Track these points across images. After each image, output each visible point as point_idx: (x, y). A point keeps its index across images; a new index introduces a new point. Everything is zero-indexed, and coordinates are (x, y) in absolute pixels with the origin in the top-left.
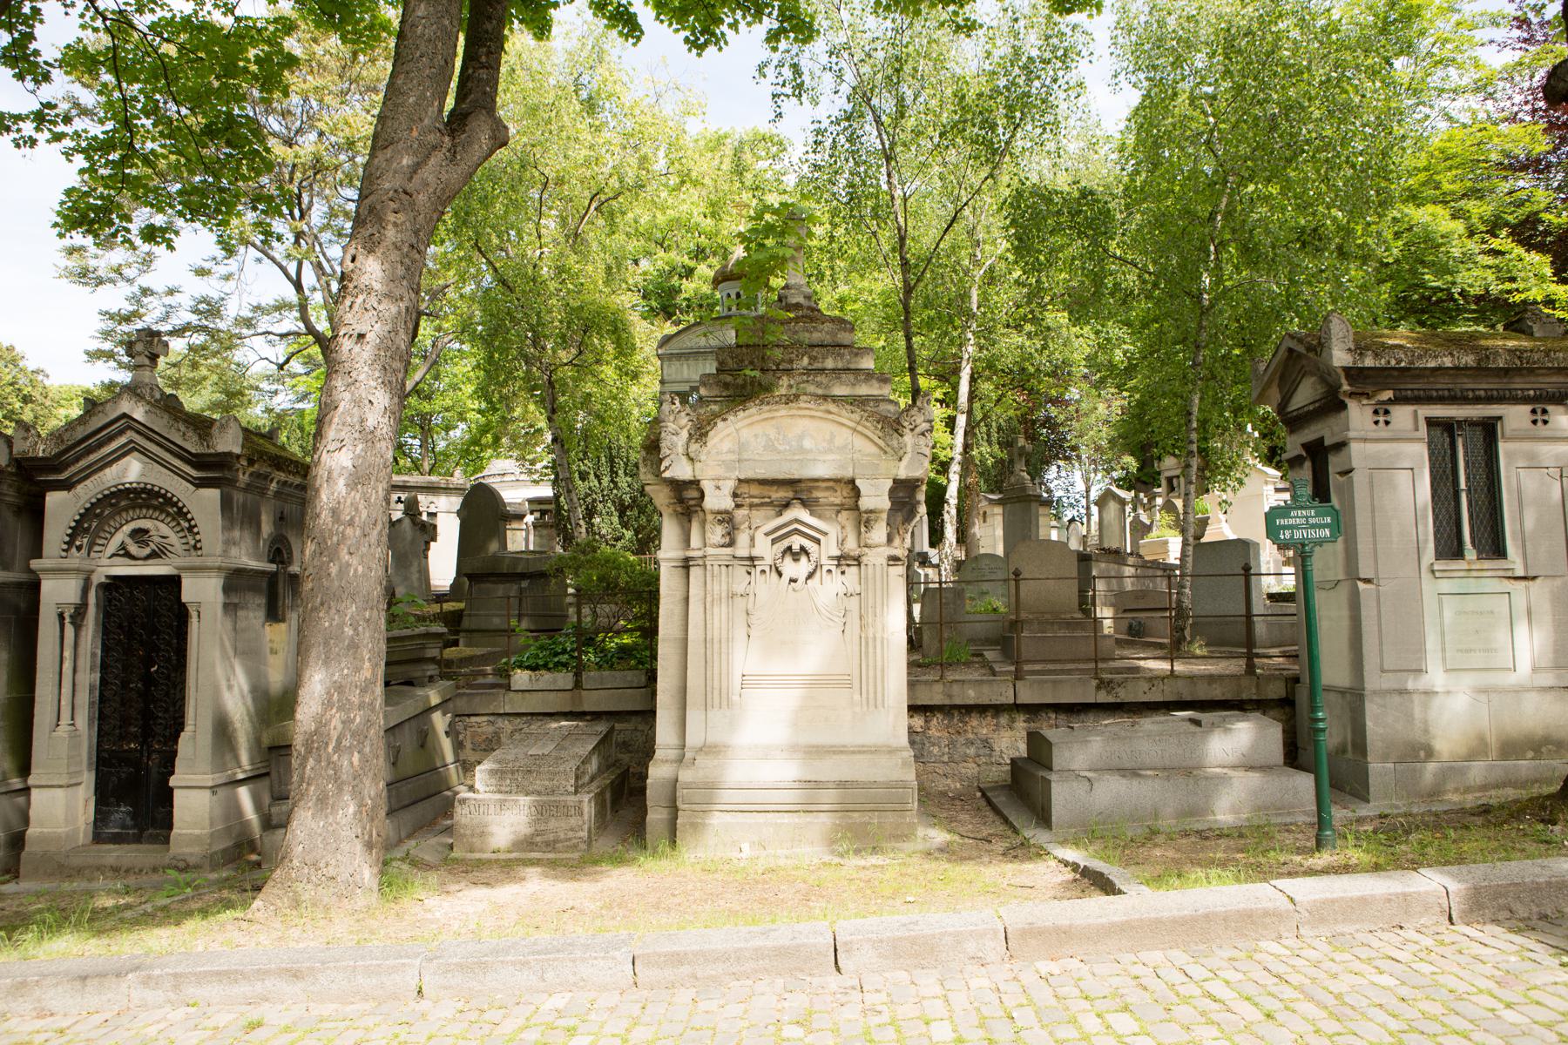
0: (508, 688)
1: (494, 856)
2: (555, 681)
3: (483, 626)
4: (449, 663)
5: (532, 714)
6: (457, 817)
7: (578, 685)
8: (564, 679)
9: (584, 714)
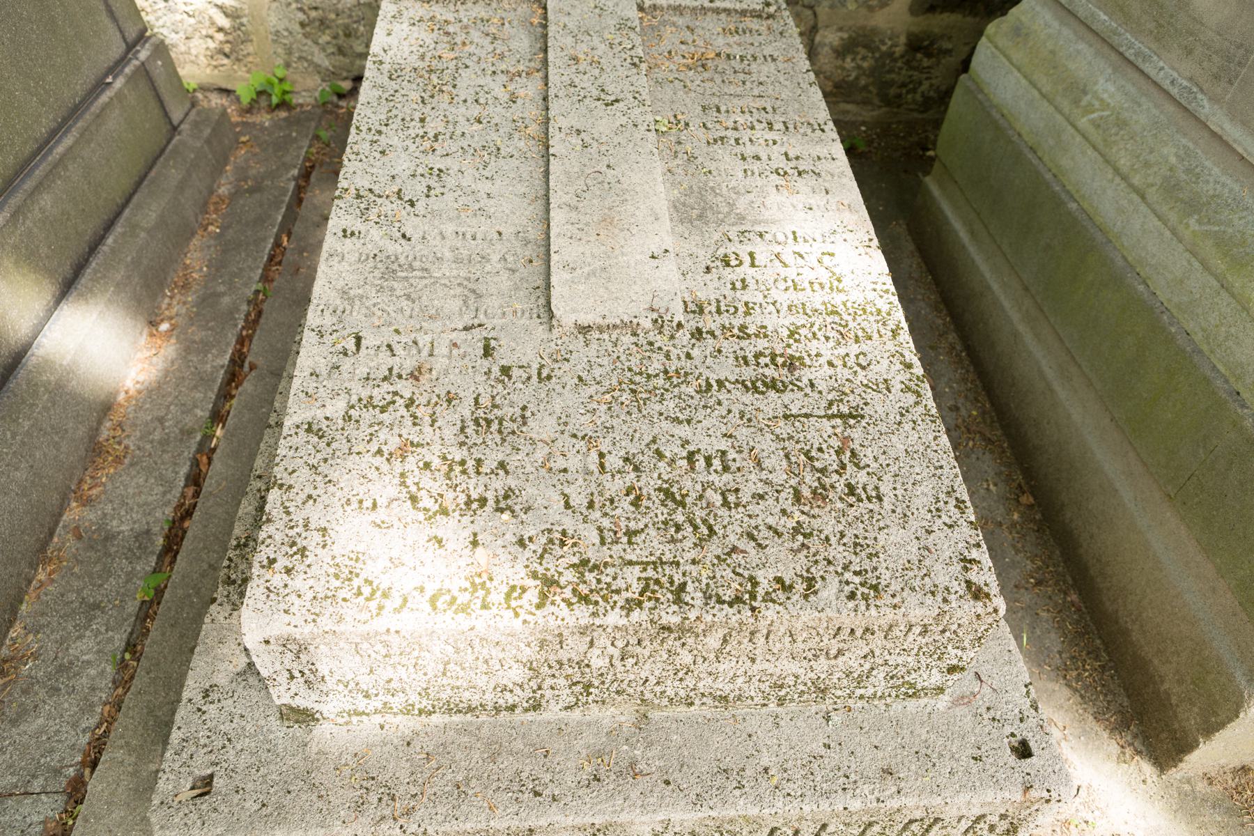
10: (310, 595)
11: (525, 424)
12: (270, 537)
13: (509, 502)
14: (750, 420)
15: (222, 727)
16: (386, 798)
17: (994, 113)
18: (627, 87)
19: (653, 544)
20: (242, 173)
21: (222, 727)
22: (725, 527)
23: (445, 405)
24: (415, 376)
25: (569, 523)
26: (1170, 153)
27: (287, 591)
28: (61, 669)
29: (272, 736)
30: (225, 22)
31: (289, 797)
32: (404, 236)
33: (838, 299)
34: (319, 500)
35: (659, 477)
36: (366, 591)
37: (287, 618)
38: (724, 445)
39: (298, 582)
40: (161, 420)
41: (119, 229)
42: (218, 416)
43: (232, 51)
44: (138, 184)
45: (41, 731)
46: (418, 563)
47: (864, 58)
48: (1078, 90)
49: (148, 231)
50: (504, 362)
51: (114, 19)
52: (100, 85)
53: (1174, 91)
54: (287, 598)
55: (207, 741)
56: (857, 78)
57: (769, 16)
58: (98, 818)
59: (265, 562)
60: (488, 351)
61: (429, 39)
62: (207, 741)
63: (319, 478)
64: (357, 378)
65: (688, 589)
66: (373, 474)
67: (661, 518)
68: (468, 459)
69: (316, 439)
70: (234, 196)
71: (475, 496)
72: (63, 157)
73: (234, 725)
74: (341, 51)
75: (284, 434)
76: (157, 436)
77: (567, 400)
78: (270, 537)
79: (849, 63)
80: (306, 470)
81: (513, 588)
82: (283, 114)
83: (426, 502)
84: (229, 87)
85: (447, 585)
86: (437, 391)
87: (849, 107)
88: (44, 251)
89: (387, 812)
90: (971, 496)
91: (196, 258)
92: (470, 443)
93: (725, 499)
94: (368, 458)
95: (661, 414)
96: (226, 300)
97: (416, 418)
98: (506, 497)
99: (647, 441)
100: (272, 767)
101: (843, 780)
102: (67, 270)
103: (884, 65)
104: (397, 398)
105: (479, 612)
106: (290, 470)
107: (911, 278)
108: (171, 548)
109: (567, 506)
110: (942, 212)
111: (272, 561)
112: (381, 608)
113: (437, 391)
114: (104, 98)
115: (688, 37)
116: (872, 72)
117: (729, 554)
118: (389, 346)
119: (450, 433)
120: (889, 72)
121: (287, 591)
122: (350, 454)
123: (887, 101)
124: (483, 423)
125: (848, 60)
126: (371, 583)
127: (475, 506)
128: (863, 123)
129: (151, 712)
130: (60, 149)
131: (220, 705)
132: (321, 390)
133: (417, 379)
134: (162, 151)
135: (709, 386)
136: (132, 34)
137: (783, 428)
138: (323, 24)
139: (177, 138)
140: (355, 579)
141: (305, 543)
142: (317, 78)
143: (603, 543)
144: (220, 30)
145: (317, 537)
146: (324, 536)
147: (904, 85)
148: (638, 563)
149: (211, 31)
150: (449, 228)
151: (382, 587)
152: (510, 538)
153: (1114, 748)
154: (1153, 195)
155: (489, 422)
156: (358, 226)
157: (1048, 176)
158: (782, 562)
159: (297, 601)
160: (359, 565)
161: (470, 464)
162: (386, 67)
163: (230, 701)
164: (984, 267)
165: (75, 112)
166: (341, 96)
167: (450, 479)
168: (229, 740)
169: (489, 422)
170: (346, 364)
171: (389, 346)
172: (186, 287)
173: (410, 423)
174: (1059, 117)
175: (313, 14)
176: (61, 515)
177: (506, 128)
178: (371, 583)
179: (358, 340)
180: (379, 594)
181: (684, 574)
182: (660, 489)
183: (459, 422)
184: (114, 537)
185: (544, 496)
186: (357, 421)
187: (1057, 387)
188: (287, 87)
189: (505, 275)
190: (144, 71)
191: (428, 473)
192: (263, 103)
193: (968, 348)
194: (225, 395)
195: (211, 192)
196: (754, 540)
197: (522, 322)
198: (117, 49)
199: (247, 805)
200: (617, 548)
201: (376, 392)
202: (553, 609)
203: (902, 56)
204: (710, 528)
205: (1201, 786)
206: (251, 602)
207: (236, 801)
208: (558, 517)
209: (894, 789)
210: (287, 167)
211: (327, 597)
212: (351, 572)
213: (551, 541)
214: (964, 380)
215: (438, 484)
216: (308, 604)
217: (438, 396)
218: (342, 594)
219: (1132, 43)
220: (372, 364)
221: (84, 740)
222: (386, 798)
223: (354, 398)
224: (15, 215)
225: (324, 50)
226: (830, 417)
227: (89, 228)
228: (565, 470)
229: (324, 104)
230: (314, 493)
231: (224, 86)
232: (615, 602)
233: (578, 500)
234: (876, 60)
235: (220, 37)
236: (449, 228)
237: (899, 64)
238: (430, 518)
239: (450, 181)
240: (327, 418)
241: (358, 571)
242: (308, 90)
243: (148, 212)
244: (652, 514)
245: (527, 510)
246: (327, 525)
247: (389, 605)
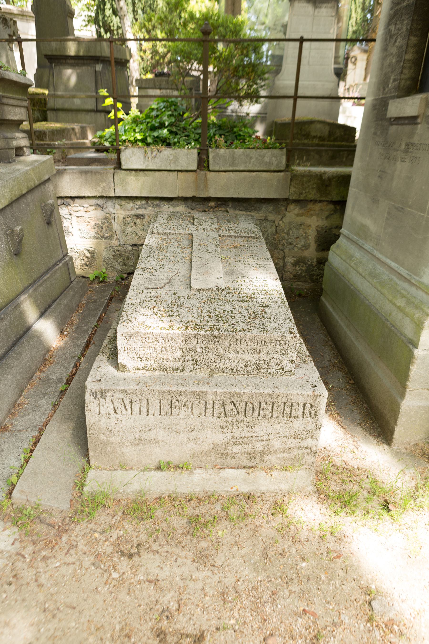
0: (118, 165)
1: (158, 483)
2: (176, 159)
3: (66, 106)
4: (41, 135)
5: (147, 198)
6: (331, 253)
7: (203, 163)
8: (186, 156)
9: (208, 199)
17: (334, 270)
18: (214, 249)
20: (89, 298)
26: (370, 266)
28: (36, 406)
30: (88, 255)
33: (266, 288)
40: (65, 355)
41: (56, 304)
42: (82, 355)
43: (89, 264)
44: (62, 293)
45: (30, 419)
47: (303, 266)
48: (351, 257)
49: (64, 305)
51: (62, 248)
52: (56, 264)
53: (369, 250)
56: (301, 273)
57: (257, 238)
58: (49, 435)
61: (160, 241)
70: (87, 304)
72: (47, 279)
74: (125, 264)
76: (64, 358)
79: (298, 268)
82: (103, 284)
84: (86, 276)
87: (300, 283)
88: (39, 302)
90: (294, 318)
91: (75, 318)
96: (85, 328)
102: (43, 310)
103: (310, 269)
107: (318, 328)
108: (68, 382)
110: (325, 305)
114: (57, 267)
115: (233, 242)
116: (306, 271)
120: (313, 271)
123: (313, 281)
125: (297, 267)
128: (305, 289)
129: (63, 415)
130: (46, 277)
134: (68, 287)
135: (230, 301)
136: (65, 253)
137: (248, 308)
138: (120, 255)
139: (72, 285)
142: (116, 273)
144: (87, 257)
147: (318, 275)
149: (83, 258)
150: (165, 274)
153: (375, 442)
154: (367, 277)
156: (142, 273)
157: (347, 282)
162: (149, 246)
164: (336, 317)
165: (50, 269)
166: (123, 279)
172: (72, 324)
174: (390, 298)
175: (118, 252)
176: (34, 374)
177: (180, 258)
184: (51, 379)
187: (355, 342)
188: (106, 275)
190: (66, 263)
192: (97, 280)
193: (335, 345)
194: (84, 350)
195: (80, 302)
198: (61, 256)
203: (316, 266)
205: (403, 451)
210: (105, 297)
214: (334, 353)
219: (361, 242)
221: (43, 421)
224: (35, 289)
225: (119, 264)
227: (50, 300)
229: (117, 281)
231: (84, 275)
234: (307, 267)
235: (86, 259)
236: (165, 274)
237: (315, 268)
239: (166, 267)
242: (112, 276)
243: (64, 301)
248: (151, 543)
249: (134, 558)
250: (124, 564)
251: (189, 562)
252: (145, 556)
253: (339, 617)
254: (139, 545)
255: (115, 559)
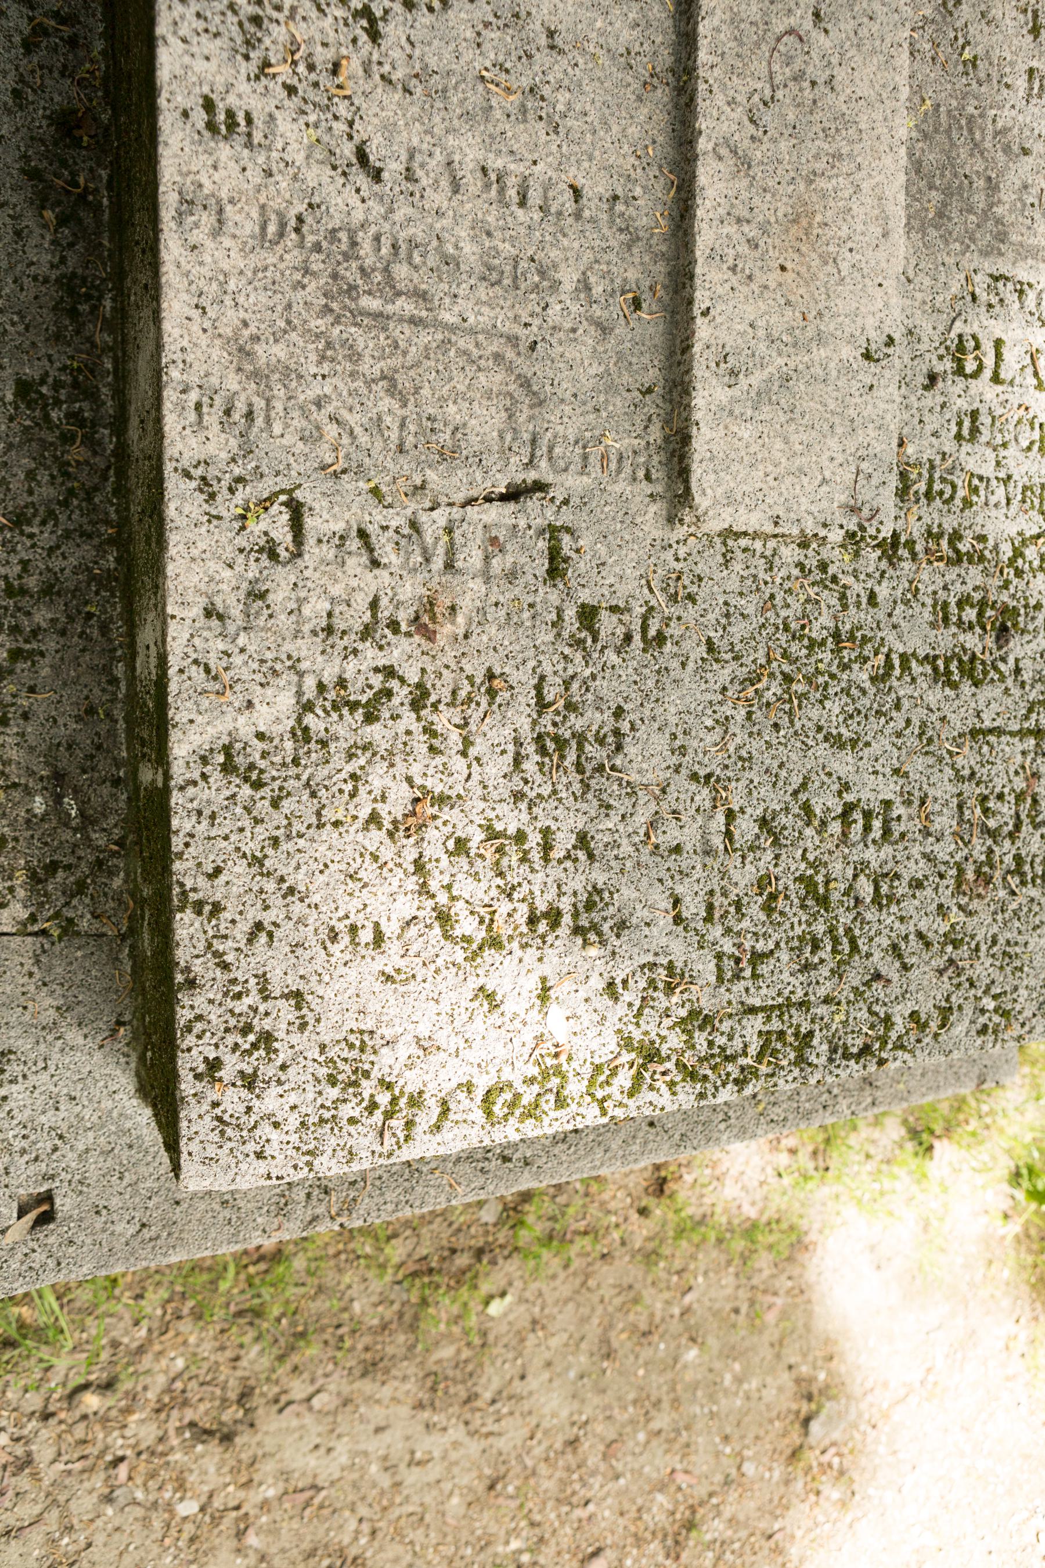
10: (294, 1120)
11: (619, 748)
12: (199, 1018)
13: (596, 916)
14: (930, 741)
15: (43, 1119)
16: (316, 1192)
19: (782, 977)
21: (43, 1119)
22: (871, 940)
23: (484, 701)
24: (423, 625)
25: (679, 951)
27: (254, 1118)
29: (128, 1124)
31: (178, 1209)
32: (362, 156)
34: (278, 934)
35: (804, 857)
36: (383, 1099)
37: (262, 1167)
38: (889, 790)
39: (270, 1101)
46: (462, 1045)
50: (585, 596)
54: (258, 1132)
55: (25, 1144)
59: (202, 1068)
60: (556, 567)
62: (25, 1144)
63: (270, 886)
64: (306, 628)
65: (815, 1042)
66: (368, 872)
67: (798, 931)
68: (528, 830)
69: (246, 791)
71: (542, 906)
73: (62, 1114)
75: (177, 780)
77: (687, 695)
78: (199, 1018)
80: (241, 867)
81: (598, 1069)
83: (467, 926)
85: (507, 1075)
86: (469, 669)
89: (321, 1210)
92: (532, 794)
93: (877, 888)
94: (353, 833)
95: (820, 729)
97: (434, 734)
98: (590, 906)
99: (795, 786)
100: (143, 1170)
101: (826, 1096)
104: (394, 684)
105: (553, 1114)
106: (209, 869)
109: (678, 920)
111: (214, 1065)
112: (409, 1124)
113: (469, 669)
117: (867, 984)
118: (362, 534)
119: (496, 767)
121: (254, 1118)
122: (320, 826)
124: (551, 746)
126: (389, 1086)
127: (542, 927)
131: (29, 1083)
132: (238, 660)
133: (430, 636)
140: (364, 1083)
141: (267, 1024)
143: (720, 979)
145: (286, 1011)
146: (298, 1007)
148: (762, 1009)
151: (408, 1090)
152: (597, 983)
155: (561, 744)
158: (924, 988)
159: (275, 1135)
160: (368, 1057)
161: (534, 839)
163: (44, 1077)
167: (501, 874)
168: (61, 1137)
169: (561, 744)
170: (281, 584)
171: (362, 534)
173: (424, 748)
178: (389, 1086)
179: (296, 511)
180: (403, 1102)
181: (813, 1021)
182: (800, 879)
183: (511, 748)
185: (641, 897)
186: (324, 743)
189: (589, 337)
191: (463, 861)
196: (900, 956)
197: (618, 488)
199: (119, 1228)
200: (739, 987)
201: (351, 667)
202: (651, 1096)
204: (853, 942)
206: (194, 1147)
207: (99, 1226)
208: (664, 941)
209: (869, 1100)
211: (322, 1121)
212: (355, 1072)
213: (652, 983)
215: (484, 885)
216: (294, 1138)
217: (470, 678)
218: (347, 1111)
220: (336, 590)
222: (316, 1192)
223: (310, 683)
226: (1022, 734)
228: (677, 849)
230: (268, 918)
232: (728, 1074)
233: (693, 908)
238: (475, 954)
240: (260, 736)
241: (367, 1067)
244: (788, 925)
245: (621, 926)
246: (302, 986)
247: (426, 1119)
248: (284, 1380)
249: (238, 1440)
250: (208, 1466)
251: (404, 1411)
252: (270, 1423)
253: (739, 1468)
254: (245, 1396)
255: (177, 1456)
